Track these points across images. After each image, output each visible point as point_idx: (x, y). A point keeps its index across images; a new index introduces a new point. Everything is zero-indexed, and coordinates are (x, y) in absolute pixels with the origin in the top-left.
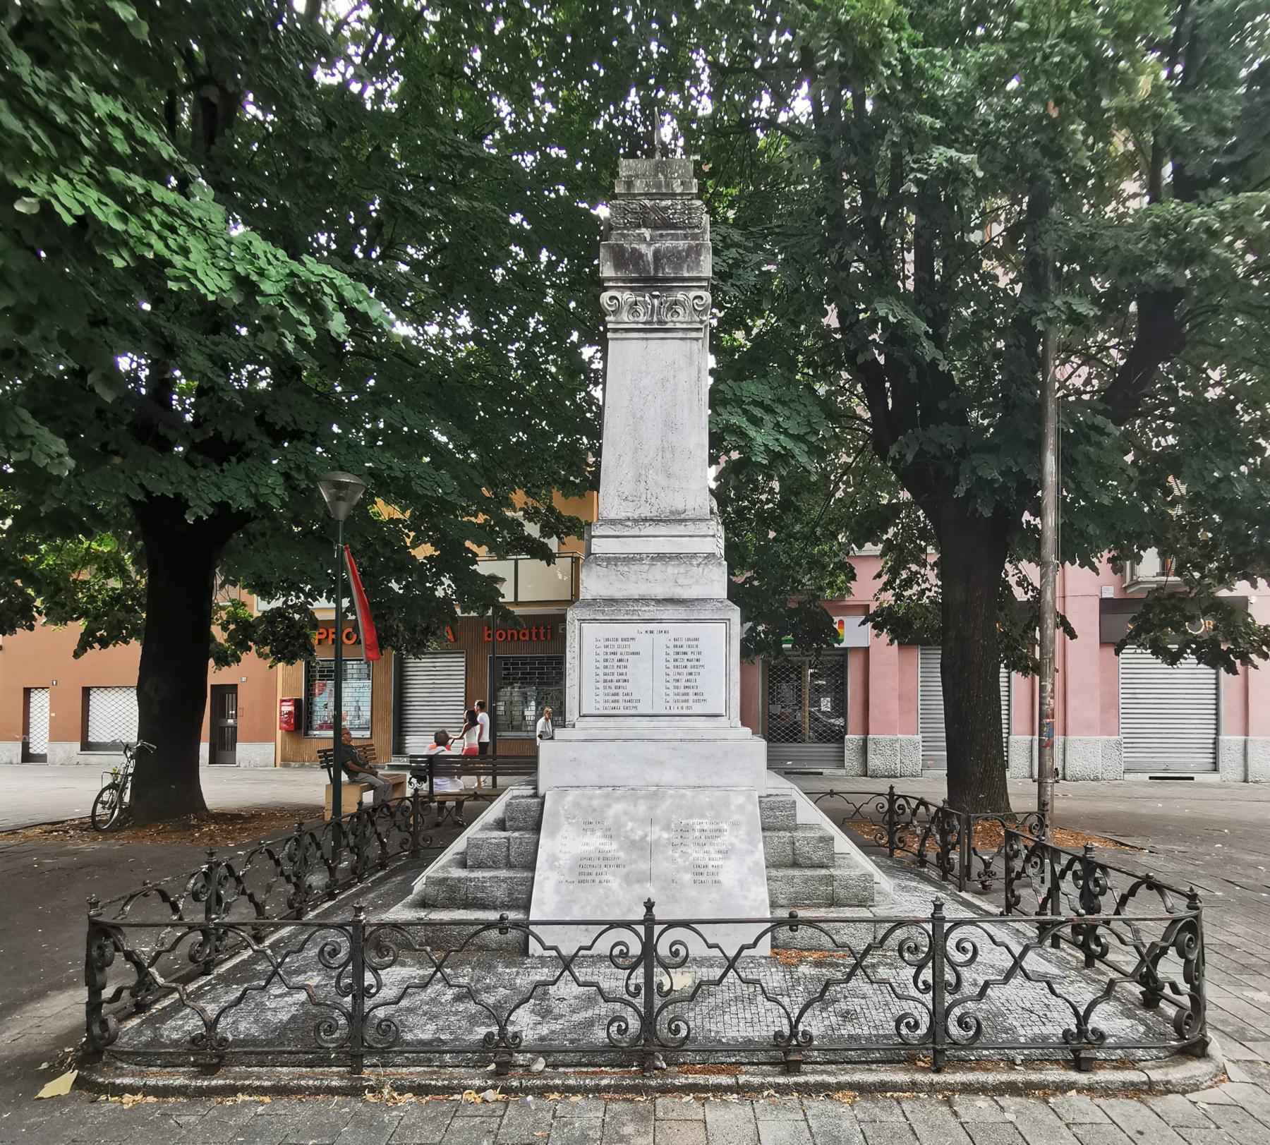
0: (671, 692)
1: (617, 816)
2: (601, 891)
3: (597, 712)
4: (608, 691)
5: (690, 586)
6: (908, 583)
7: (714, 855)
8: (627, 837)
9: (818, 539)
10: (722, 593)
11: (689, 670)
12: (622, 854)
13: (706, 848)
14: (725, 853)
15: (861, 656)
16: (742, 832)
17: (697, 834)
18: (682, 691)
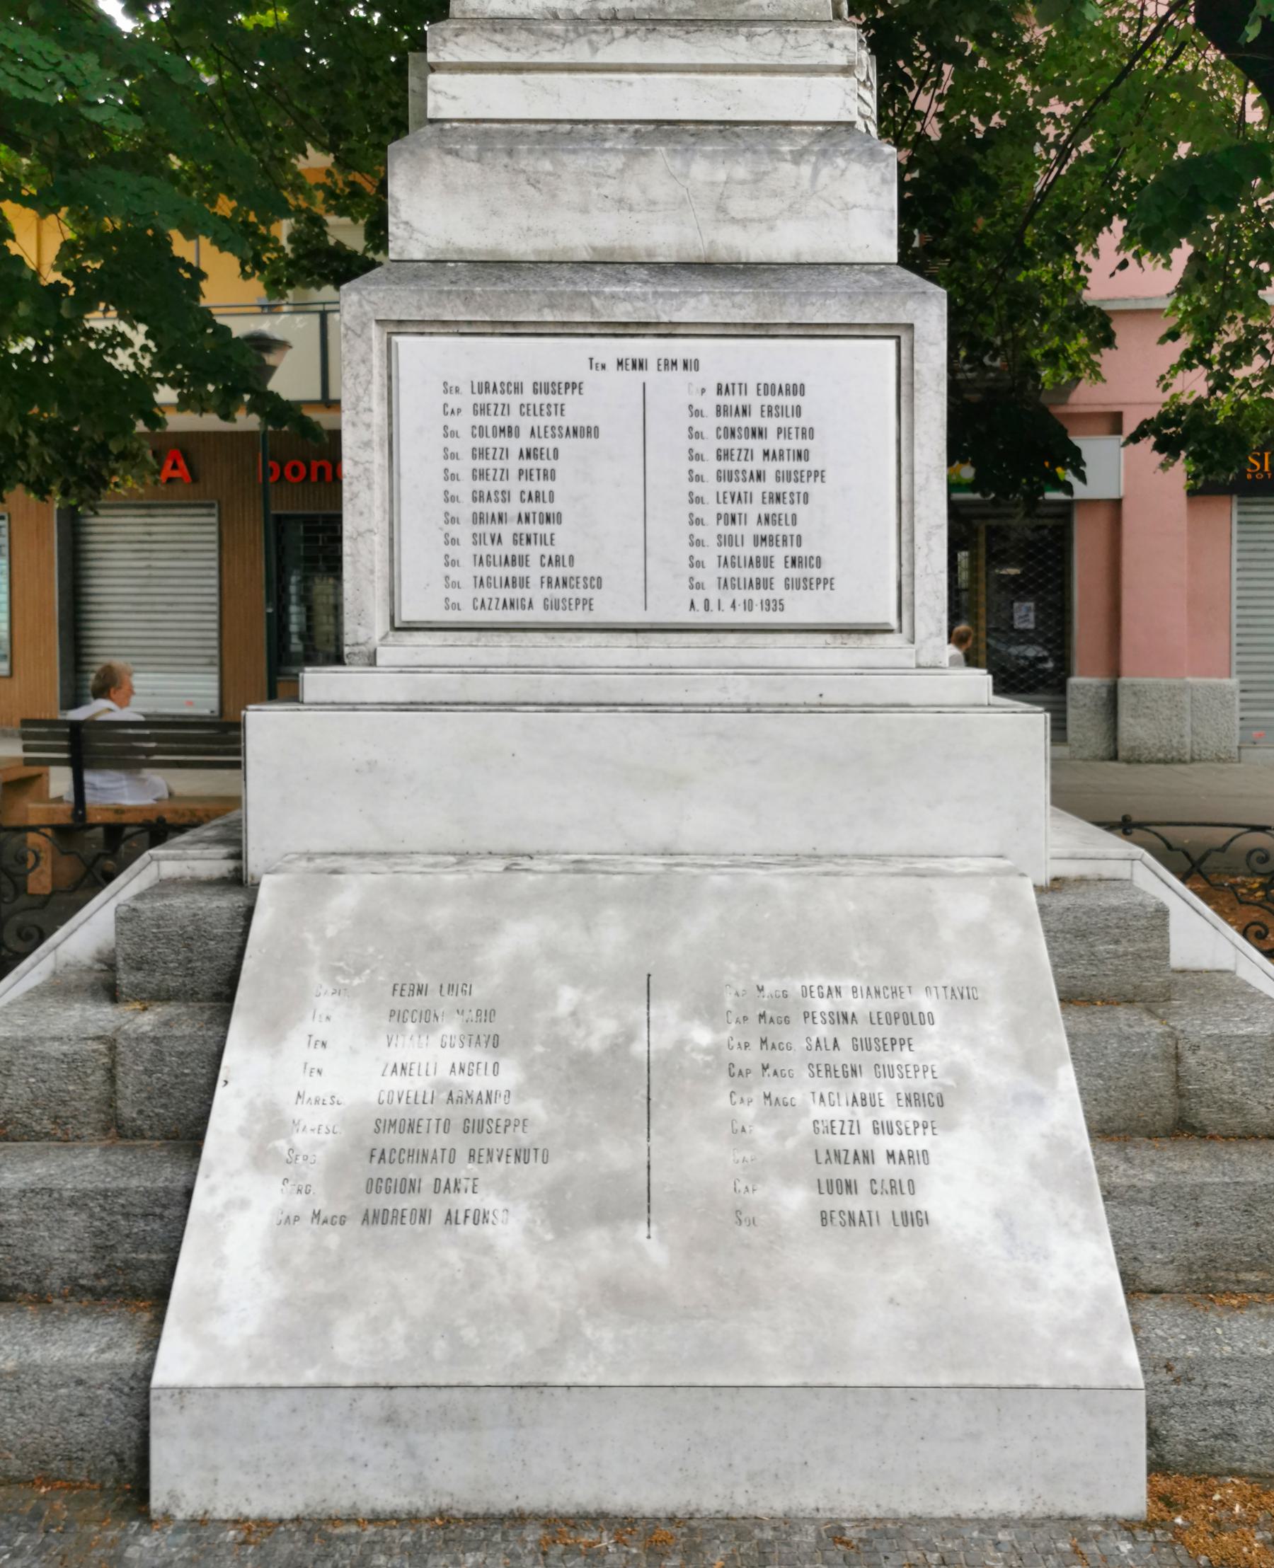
0: (710, 554)
1: (520, 966)
2: (453, 1255)
3: (452, 617)
4: (488, 549)
5: (769, 224)
6: (1240, 352)
7: (891, 1113)
8: (557, 1043)
9: (1029, 254)
10: (881, 241)
11: (771, 485)
12: (535, 1108)
13: (862, 1085)
14: (931, 1102)
15: (1102, 516)
16: (992, 1021)
17: (823, 1031)
18: (749, 550)
